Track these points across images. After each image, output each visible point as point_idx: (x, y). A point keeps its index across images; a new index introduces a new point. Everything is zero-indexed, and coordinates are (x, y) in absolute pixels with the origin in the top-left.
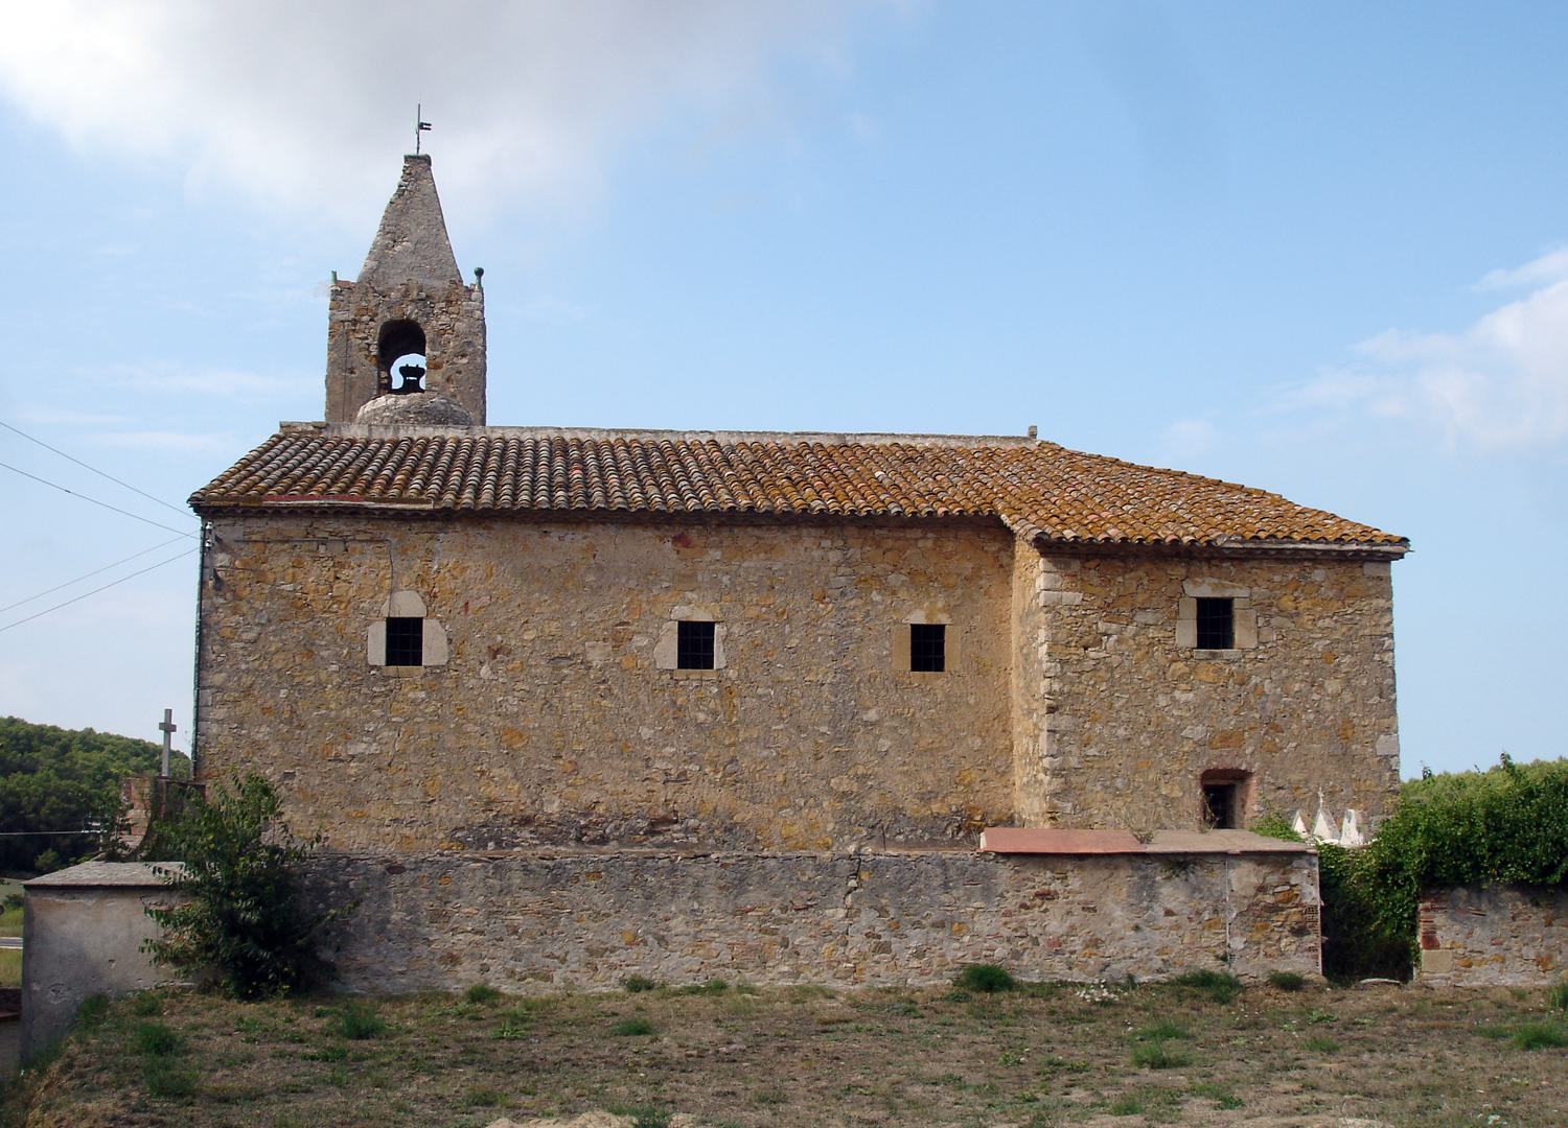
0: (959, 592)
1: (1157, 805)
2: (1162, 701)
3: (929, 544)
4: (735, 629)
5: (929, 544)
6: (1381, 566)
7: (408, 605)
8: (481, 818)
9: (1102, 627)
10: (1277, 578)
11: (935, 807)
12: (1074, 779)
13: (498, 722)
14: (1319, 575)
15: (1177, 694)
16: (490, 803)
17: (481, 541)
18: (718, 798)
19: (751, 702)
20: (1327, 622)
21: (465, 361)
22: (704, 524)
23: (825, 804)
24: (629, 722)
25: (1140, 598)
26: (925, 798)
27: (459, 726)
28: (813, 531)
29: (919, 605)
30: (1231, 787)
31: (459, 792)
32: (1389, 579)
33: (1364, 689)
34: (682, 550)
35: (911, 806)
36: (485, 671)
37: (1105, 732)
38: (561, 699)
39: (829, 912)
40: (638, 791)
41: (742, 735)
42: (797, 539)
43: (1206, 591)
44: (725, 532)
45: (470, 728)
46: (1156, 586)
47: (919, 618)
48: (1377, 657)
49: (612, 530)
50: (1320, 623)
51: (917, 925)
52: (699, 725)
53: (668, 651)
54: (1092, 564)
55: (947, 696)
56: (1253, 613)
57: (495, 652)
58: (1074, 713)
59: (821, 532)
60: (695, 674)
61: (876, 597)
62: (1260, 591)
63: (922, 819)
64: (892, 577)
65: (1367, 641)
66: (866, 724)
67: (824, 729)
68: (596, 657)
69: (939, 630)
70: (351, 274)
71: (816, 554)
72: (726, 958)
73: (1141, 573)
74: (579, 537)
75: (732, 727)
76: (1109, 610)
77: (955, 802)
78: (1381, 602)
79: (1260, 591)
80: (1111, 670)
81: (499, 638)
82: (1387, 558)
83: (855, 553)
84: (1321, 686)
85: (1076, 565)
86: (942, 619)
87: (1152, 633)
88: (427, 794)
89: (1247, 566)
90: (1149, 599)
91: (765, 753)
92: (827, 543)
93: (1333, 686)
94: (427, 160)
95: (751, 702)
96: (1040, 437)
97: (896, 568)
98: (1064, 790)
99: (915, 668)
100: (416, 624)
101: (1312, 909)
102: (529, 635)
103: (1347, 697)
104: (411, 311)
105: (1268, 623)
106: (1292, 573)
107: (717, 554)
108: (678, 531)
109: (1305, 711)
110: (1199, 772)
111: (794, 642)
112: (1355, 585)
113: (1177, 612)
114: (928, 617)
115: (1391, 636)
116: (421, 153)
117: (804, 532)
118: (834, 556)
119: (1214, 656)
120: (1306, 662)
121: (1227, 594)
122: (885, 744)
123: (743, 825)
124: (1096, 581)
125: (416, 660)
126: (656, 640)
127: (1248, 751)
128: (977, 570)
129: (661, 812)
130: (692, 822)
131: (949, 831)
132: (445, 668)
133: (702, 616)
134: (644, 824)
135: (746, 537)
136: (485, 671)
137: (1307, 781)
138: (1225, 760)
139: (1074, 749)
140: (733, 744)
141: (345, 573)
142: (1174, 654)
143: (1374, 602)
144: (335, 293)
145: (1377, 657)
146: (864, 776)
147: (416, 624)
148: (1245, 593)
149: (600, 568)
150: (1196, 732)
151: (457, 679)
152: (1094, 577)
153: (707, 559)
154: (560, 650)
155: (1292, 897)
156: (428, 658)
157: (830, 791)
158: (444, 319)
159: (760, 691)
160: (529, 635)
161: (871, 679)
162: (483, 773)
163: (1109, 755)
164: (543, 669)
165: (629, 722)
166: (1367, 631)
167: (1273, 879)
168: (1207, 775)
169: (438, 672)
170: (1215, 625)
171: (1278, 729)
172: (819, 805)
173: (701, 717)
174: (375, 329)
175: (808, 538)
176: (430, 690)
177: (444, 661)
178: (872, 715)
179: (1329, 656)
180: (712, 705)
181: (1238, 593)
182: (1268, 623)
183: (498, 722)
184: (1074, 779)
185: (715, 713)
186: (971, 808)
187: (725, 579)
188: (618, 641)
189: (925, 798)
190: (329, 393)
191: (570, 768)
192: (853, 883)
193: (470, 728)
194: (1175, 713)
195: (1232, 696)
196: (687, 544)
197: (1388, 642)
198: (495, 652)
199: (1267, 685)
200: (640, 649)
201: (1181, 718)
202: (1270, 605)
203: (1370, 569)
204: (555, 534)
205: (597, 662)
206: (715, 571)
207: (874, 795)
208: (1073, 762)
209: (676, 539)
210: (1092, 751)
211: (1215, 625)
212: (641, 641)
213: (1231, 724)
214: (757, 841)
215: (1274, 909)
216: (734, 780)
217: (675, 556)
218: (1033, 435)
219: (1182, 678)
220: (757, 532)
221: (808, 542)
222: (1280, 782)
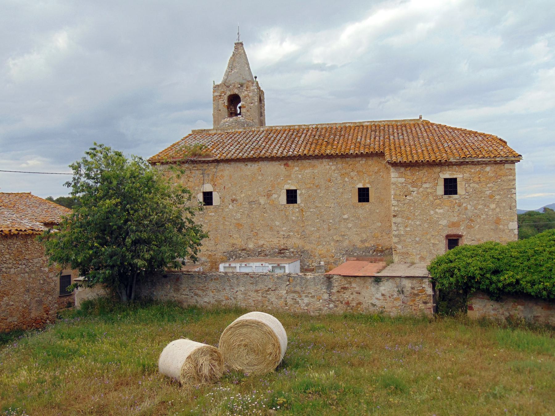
0: (373, 177)
1: (430, 246)
2: (432, 212)
3: (364, 162)
4: (303, 191)
5: (364, 162)
6: (512, 165)
7: (208, 188)
8: (231, 249)
9: (411, 189)
10: (473, 171)
11: (366, 245)
12: (402, 238)
13: (235, 221)
14: (488, 169)
15: (437, 210)
16: (233, 245)
17: (228, 168)
18: (300, 243)
19: (309, 213)
20: (491, 185)
21: (252, 105)
22: (293, 160)
23: (332, 244)
24: (273, 220)
25: (424, 179)
26: (363, 242)
27: (224, 222)
28: (327, 160)
29: (360, 182)
30: (458, 240)
31: (224, 242)
32: (514, 169)
33: (504, 207)
34: (287, 168)
35: (359, 244)
36: (230, 207)
37: (412, 223)
38: (252, 214)
39: (281, 292)
40: (276, 241)
41: (306, 224)
42: (322, 163)
43: (447, 176)
44: (299, 162)
45: (227, 223)
46: (430, 175)
47: (361, 186)
48: (509, 196)
49: (266, 163)
50: (488, 185)
51: (306, 296)
52: (293, 221)
53: (283, 198)
54: (409, 168)
55: (370, 210)
56: (464, 183)
57: (233, 201)
58: (402, 217)
59: (329, 160)
60: (291, 205)
61: (346, 179)
62: (467, 175)
63: (362, 249)
64: (352, 173)
65: (505, 191)
66: (344, 219)
67: (331, 221)
68: (262, 201)
69: (367, 189)
70: (219, 82)
71: (328, 167)
72: (253, 304)
73: (424, 171)
74: (256, 165)
75: (303, 221)
76: (414, 184)
77: (372, 243)
78: (511, 177)
79: (467, 175)
80: (414, 203)
81: (234, 196)
82: (513, 162)
83: (340, 166)
84: (488, 206)
85: (402, 169)
86: (368, 186)
87: (429, 190)
88: (215, 242)
89: (462, 167)
90: (427, 179)
91: (313, 229)
92: (331, 164)
93: (493, 206)
94: (242, 44)
95: (309, 213)
96: (423, 119)
97: (353, 171)
98: (399, 242)
99: (360, 201)
100: (211, 193)
101: (430, 295)
102: (243, 195)
103: (498, 210)
104: (236, 91)
105: (469, 186)
106: (478, 168)
107: (297, 169)
108: (285, 162)
109: (482, 214)
110: (444, 235)
111: (321, 195)
112: (501, 172)
113: (437, 183)
114: (363, 185)
115: (515, 189)
116: (240, 41)
117: (324, 160)
118: (333, 168)
119: (450, 197)
120: (483, 198)
121: (455, 177)
122: (350, 225)
123: (307, 251)
124: (409, 174)
125: (211, 204)
126: (279, 196)
127: (462, 228)
128: (379, 170)
129: (282, 247)
130: (292, 250)
131: (371, 252)
132: (219, 206)
133: (293, 188)
134: (277, 250)
135: (306, 162)
136: (230, 207)
137: (483, 238)
138: (454, 231)
139: (402, 228)
140: (303, 226)
141: (191, 179)
142: (437, 197)
143: (509, 177)
144: (214, 87)
145: (509, 196)
146: (344, 235)
147: (211, 193)
148: (461, 176)
149: (262, 175)
150: (444, 222)
151: (223, 209)
152: (408, 173)
153: (294, 170)
154: (252, 199)
155: (423, 290)
156: (214, 203)
157: (333, 240)
158: (246, 93)
159: (311, 210)
160: (243, 195)
161: (346, 205)
162: (231, 236)
163: (414, 230)
164: (247, 205)
165: (273, 220)
166: (506, 187)
167: (417, 285)
168: (447, 236)
169: (217, 207)
170: (451, 186)
171: (472, 221)
172: (330, 244)
173: (294, 218)
174: (226, 97)
175: (325, 161)
176: (216, 212)
177: (219, 204)
178: (346, 216)
179: (491, 197)
180: (297, 215)
181: (459, 176)
182: (469, 186)
183: (235, 221)
184: (402, 238)
185: (298, 217)
186: (378, 245)
187: (300, 176)
188: (269, 196)
189: (363, 242)
190: (214, 118)
191: (255, 234)
192: (288, 283)
193: (227, 223)
194: (436, 216)
195: (456, 210)
196: (288, 166)
197: (513, 190)
198: (233, 201)
199: (469, 207)
200: (275, 198)
201: (438, 218)
202: (470, 180)
203: (507, 166)
204: (249, 164)
205: (263, 203)
206: (297, 174)
207: (347, 241)
208: (402, 233)
209: (285, 165)
210: (408, 229)
211: (451, 186)
212: (275, 196)
213: (455, 219)
214: (311, 255)
215: (417, 295)
216: (304, 237)
217: (284, 170)
218: (421, 118)
219: (439, 205)
220: (309, 161)
221: (325, 163)
222: (473, 238)
